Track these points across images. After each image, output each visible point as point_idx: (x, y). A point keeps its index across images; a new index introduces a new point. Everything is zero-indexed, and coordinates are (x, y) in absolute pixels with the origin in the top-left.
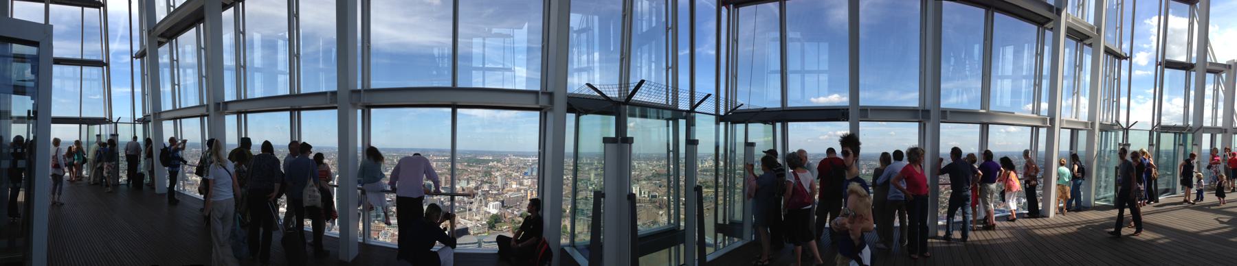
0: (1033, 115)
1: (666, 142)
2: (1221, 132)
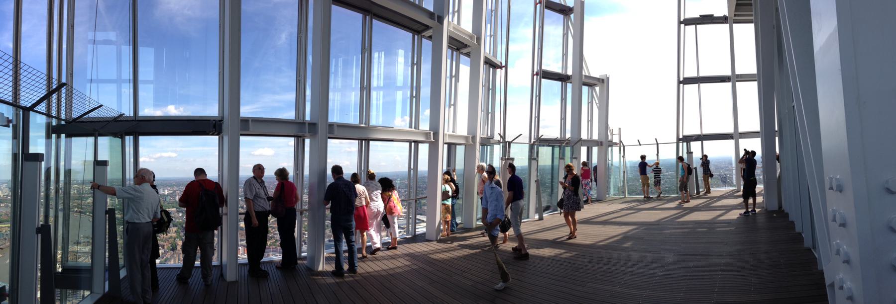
0: (411, 129)
2: (597, 145)
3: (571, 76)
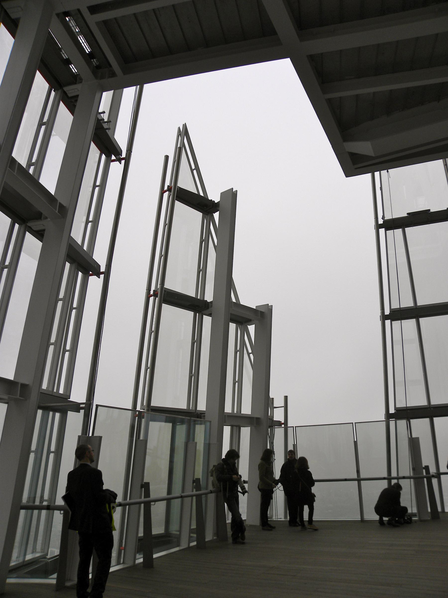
3: (211, 302)
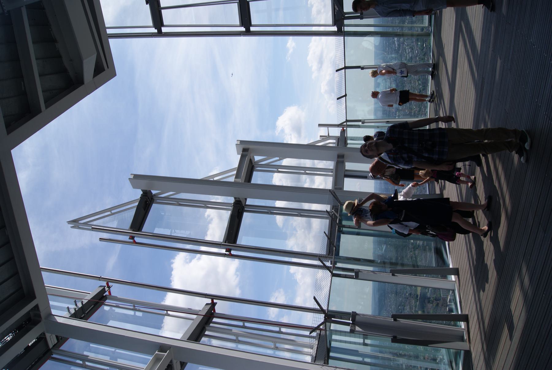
1: (329, 326)
2: (343, 163)
3: (235, 198)
